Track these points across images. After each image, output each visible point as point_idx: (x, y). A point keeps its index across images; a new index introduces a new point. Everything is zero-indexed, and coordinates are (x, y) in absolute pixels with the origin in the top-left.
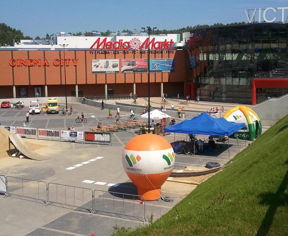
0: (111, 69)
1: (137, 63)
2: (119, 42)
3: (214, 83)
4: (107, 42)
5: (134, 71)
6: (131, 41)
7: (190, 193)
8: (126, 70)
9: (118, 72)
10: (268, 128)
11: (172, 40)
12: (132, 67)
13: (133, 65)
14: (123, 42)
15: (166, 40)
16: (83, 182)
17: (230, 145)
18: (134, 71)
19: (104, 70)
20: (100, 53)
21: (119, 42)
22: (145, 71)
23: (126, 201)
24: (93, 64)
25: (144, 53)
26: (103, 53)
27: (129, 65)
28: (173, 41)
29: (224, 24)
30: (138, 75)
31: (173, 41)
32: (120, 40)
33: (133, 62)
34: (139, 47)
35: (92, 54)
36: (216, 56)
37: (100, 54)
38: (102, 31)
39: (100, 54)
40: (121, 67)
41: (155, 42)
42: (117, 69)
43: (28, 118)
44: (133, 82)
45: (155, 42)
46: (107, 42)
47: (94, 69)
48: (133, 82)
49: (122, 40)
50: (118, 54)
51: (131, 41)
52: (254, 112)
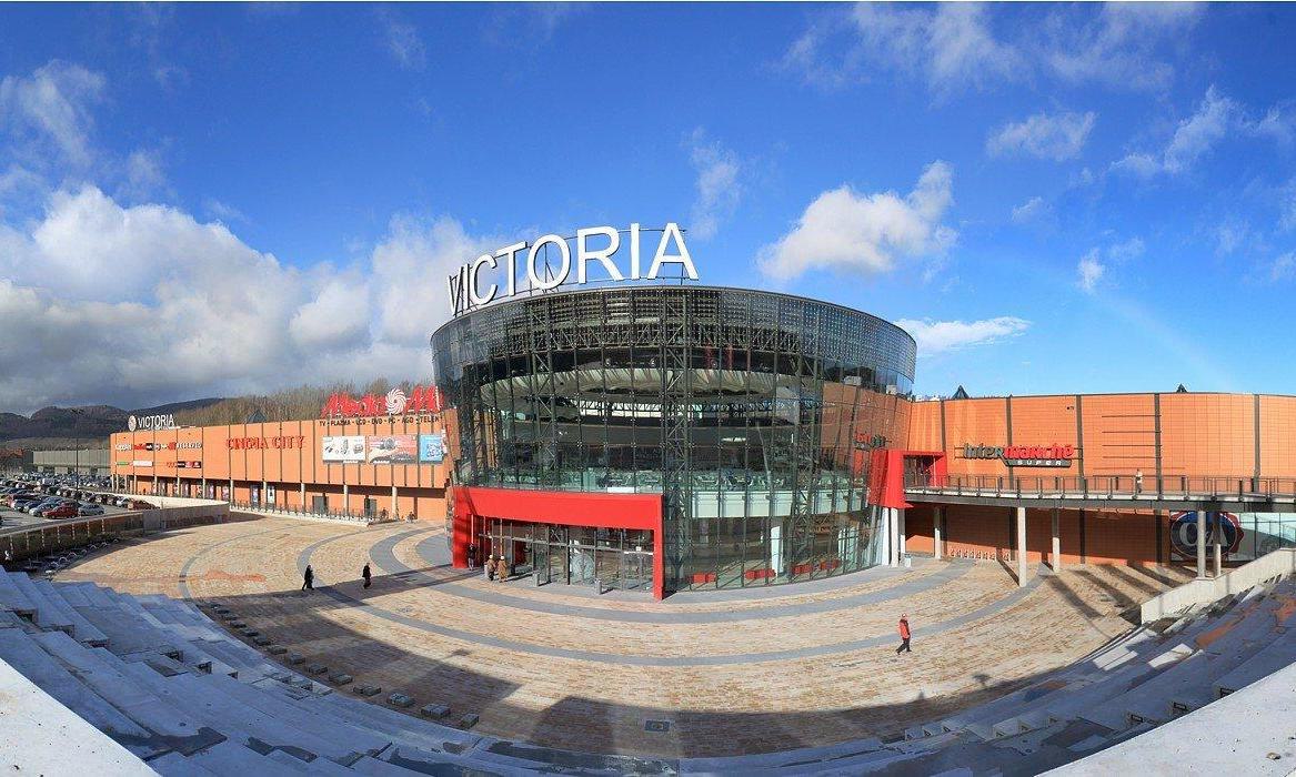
0: (352, 456)
1: (396, 443)
5: (393, 461)
7: (553, 702)
8: (376, 459)
9: (362, 461)
12: (387, 453)
13: (390, 448)
18: (392, 461)
19: (339, 457)
22: (411, 462)
24: (325, 445)
27: (382, 447)
29: (799, 42)
30: (399, 468)
33: (390, 441)
36: (143, 464)
38: (942, 395)
40: (369, 450)
42: (361, 456)
43: (384, 494)
47: (327, 456)
52: (903, 518)
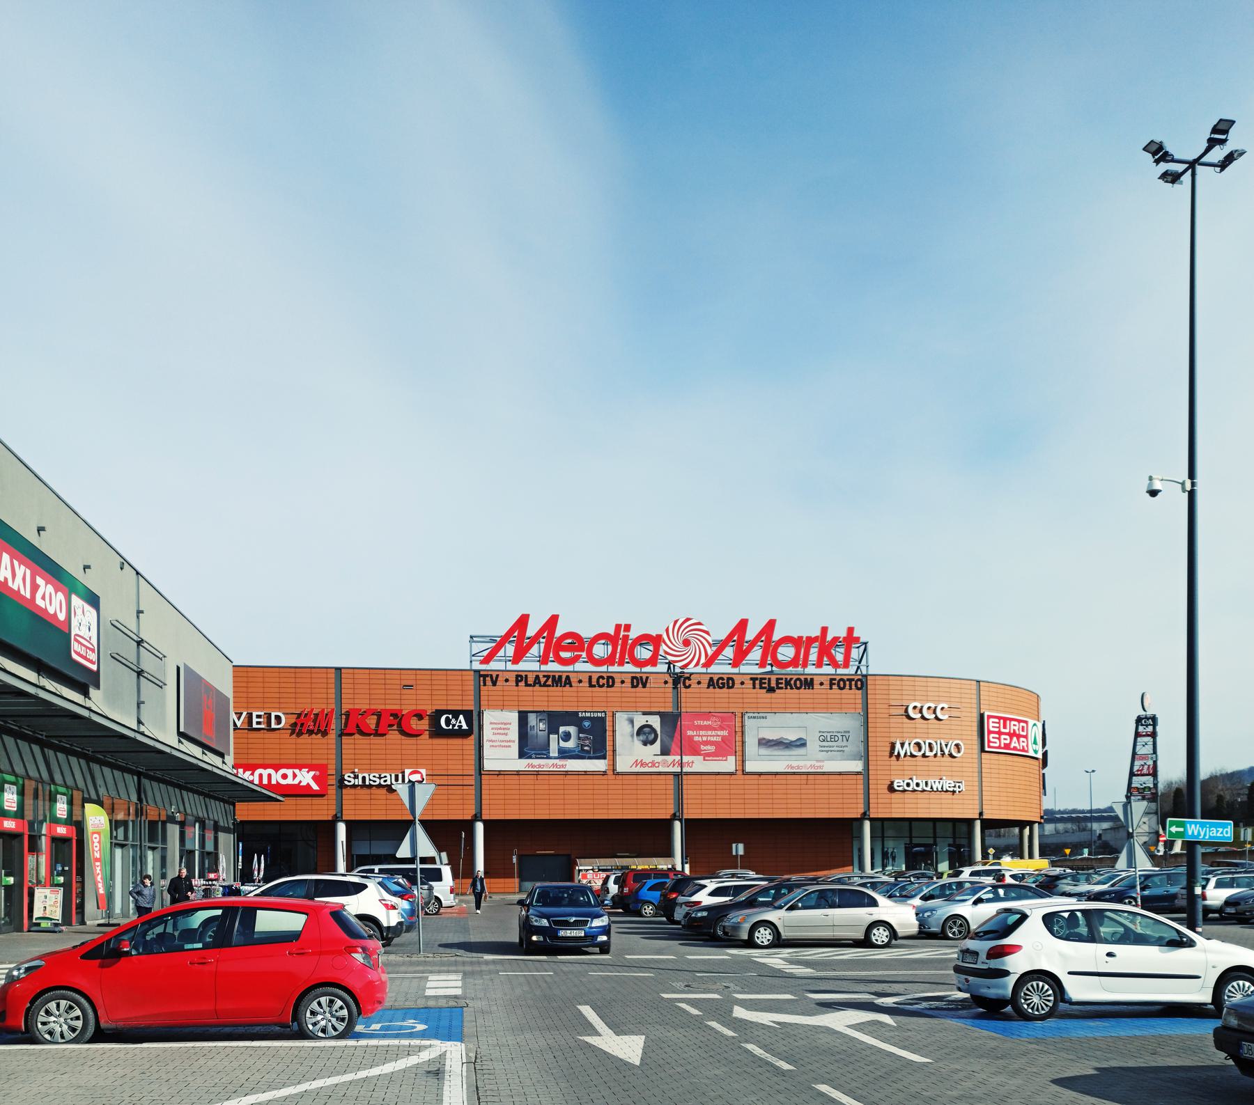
2: (612, 633)
3: (216, 839)
4: (558, 634)
10: (396, 945)
11: (851, 630)
14: (633, 634)
16: (709, 1023)
20: (531, 681)
21: (612, 633)
26: (543, 680)
28: (855, 635)
31: (855, 635)
32: (618, 627)
34: (703, 660)
39: (591, 686)
41: (776, 637)
45: (776, 637)
46: (558, 634)
49: (628, 627)
50: (609, 686)
51: (667, 630)
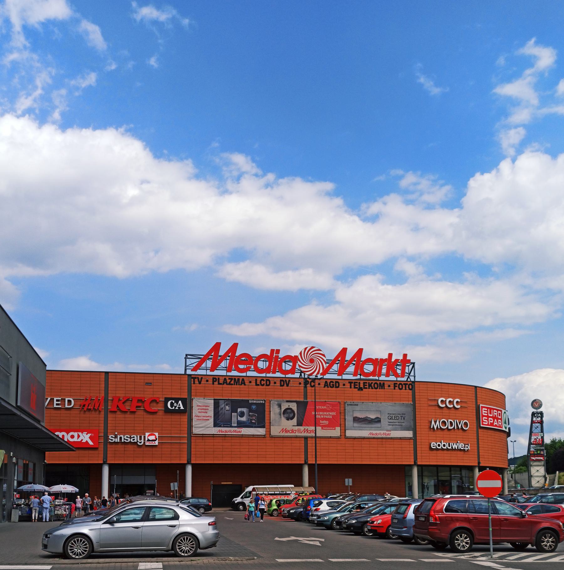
4: (238, 354)
6: (301, 353)
11: (405, 356)
14: (281, 355)
15: (390, 355)
17: (318, 464)
20: (221, 381)
21: (269, 355)
23: (179, 462)
25: (336, 387)
32: (272, 351)
34: (321, 371)
35: (200, 383)
37: (219, 384)
39: (257, 385)
44: (413, 463)
45: (363, 358)
46: (238, 354)
48: (413, 463)
49: (278, 351)
50: (267, 385)
51: (301, 353)
